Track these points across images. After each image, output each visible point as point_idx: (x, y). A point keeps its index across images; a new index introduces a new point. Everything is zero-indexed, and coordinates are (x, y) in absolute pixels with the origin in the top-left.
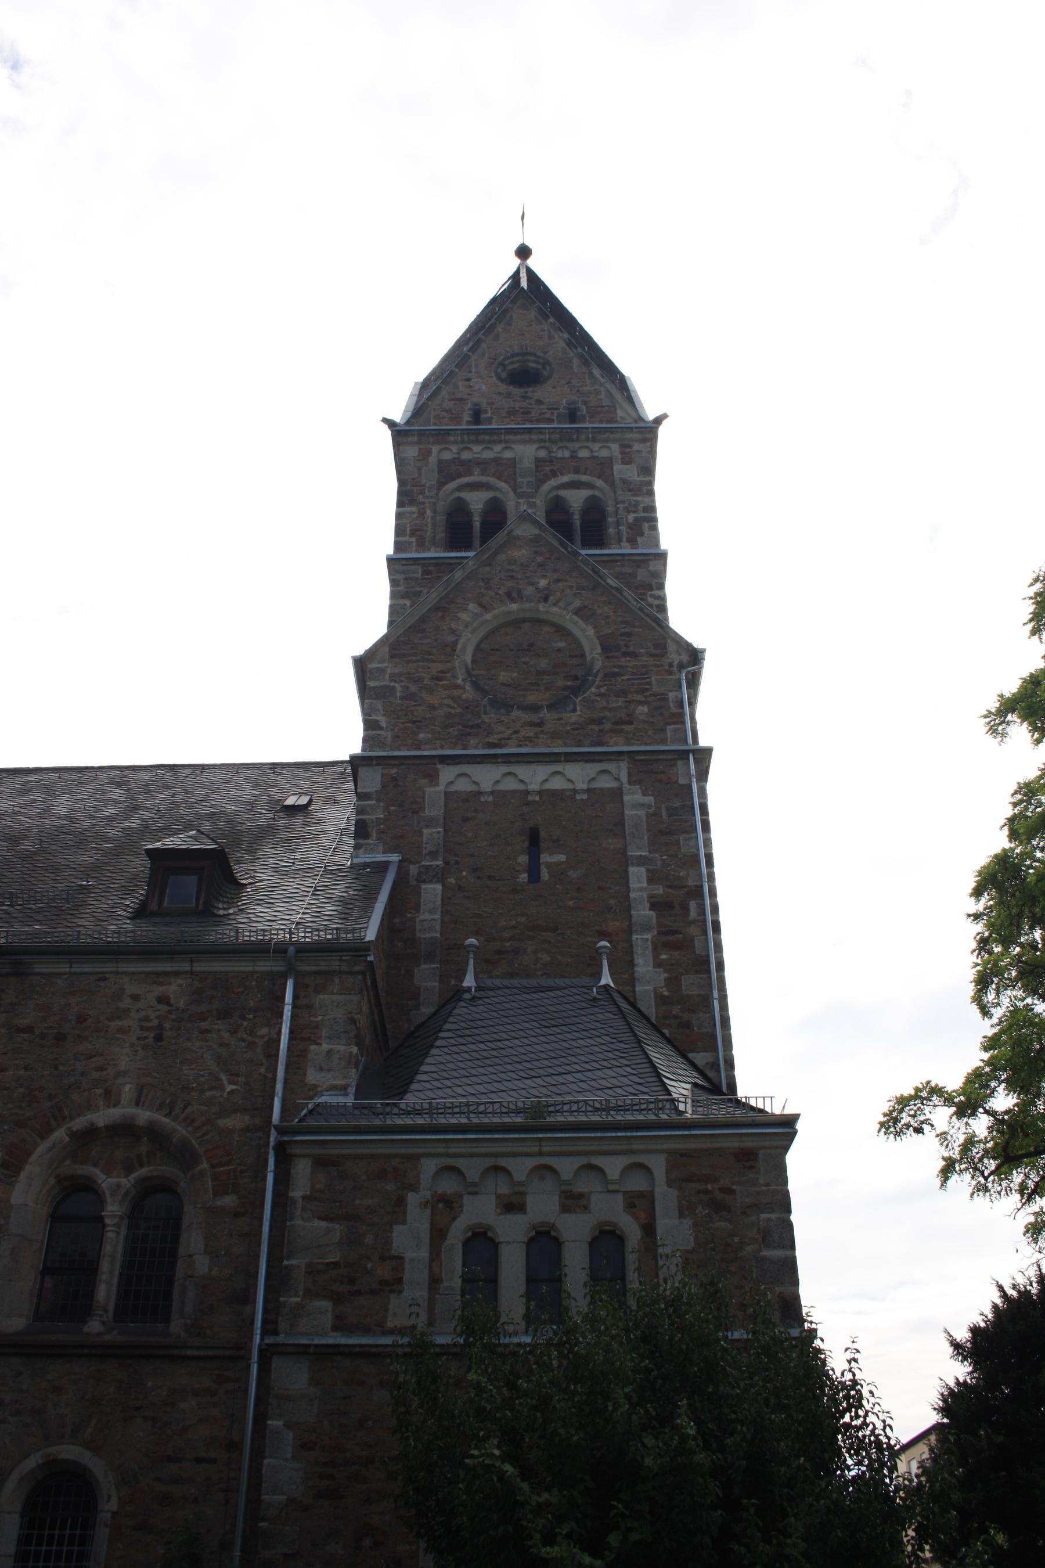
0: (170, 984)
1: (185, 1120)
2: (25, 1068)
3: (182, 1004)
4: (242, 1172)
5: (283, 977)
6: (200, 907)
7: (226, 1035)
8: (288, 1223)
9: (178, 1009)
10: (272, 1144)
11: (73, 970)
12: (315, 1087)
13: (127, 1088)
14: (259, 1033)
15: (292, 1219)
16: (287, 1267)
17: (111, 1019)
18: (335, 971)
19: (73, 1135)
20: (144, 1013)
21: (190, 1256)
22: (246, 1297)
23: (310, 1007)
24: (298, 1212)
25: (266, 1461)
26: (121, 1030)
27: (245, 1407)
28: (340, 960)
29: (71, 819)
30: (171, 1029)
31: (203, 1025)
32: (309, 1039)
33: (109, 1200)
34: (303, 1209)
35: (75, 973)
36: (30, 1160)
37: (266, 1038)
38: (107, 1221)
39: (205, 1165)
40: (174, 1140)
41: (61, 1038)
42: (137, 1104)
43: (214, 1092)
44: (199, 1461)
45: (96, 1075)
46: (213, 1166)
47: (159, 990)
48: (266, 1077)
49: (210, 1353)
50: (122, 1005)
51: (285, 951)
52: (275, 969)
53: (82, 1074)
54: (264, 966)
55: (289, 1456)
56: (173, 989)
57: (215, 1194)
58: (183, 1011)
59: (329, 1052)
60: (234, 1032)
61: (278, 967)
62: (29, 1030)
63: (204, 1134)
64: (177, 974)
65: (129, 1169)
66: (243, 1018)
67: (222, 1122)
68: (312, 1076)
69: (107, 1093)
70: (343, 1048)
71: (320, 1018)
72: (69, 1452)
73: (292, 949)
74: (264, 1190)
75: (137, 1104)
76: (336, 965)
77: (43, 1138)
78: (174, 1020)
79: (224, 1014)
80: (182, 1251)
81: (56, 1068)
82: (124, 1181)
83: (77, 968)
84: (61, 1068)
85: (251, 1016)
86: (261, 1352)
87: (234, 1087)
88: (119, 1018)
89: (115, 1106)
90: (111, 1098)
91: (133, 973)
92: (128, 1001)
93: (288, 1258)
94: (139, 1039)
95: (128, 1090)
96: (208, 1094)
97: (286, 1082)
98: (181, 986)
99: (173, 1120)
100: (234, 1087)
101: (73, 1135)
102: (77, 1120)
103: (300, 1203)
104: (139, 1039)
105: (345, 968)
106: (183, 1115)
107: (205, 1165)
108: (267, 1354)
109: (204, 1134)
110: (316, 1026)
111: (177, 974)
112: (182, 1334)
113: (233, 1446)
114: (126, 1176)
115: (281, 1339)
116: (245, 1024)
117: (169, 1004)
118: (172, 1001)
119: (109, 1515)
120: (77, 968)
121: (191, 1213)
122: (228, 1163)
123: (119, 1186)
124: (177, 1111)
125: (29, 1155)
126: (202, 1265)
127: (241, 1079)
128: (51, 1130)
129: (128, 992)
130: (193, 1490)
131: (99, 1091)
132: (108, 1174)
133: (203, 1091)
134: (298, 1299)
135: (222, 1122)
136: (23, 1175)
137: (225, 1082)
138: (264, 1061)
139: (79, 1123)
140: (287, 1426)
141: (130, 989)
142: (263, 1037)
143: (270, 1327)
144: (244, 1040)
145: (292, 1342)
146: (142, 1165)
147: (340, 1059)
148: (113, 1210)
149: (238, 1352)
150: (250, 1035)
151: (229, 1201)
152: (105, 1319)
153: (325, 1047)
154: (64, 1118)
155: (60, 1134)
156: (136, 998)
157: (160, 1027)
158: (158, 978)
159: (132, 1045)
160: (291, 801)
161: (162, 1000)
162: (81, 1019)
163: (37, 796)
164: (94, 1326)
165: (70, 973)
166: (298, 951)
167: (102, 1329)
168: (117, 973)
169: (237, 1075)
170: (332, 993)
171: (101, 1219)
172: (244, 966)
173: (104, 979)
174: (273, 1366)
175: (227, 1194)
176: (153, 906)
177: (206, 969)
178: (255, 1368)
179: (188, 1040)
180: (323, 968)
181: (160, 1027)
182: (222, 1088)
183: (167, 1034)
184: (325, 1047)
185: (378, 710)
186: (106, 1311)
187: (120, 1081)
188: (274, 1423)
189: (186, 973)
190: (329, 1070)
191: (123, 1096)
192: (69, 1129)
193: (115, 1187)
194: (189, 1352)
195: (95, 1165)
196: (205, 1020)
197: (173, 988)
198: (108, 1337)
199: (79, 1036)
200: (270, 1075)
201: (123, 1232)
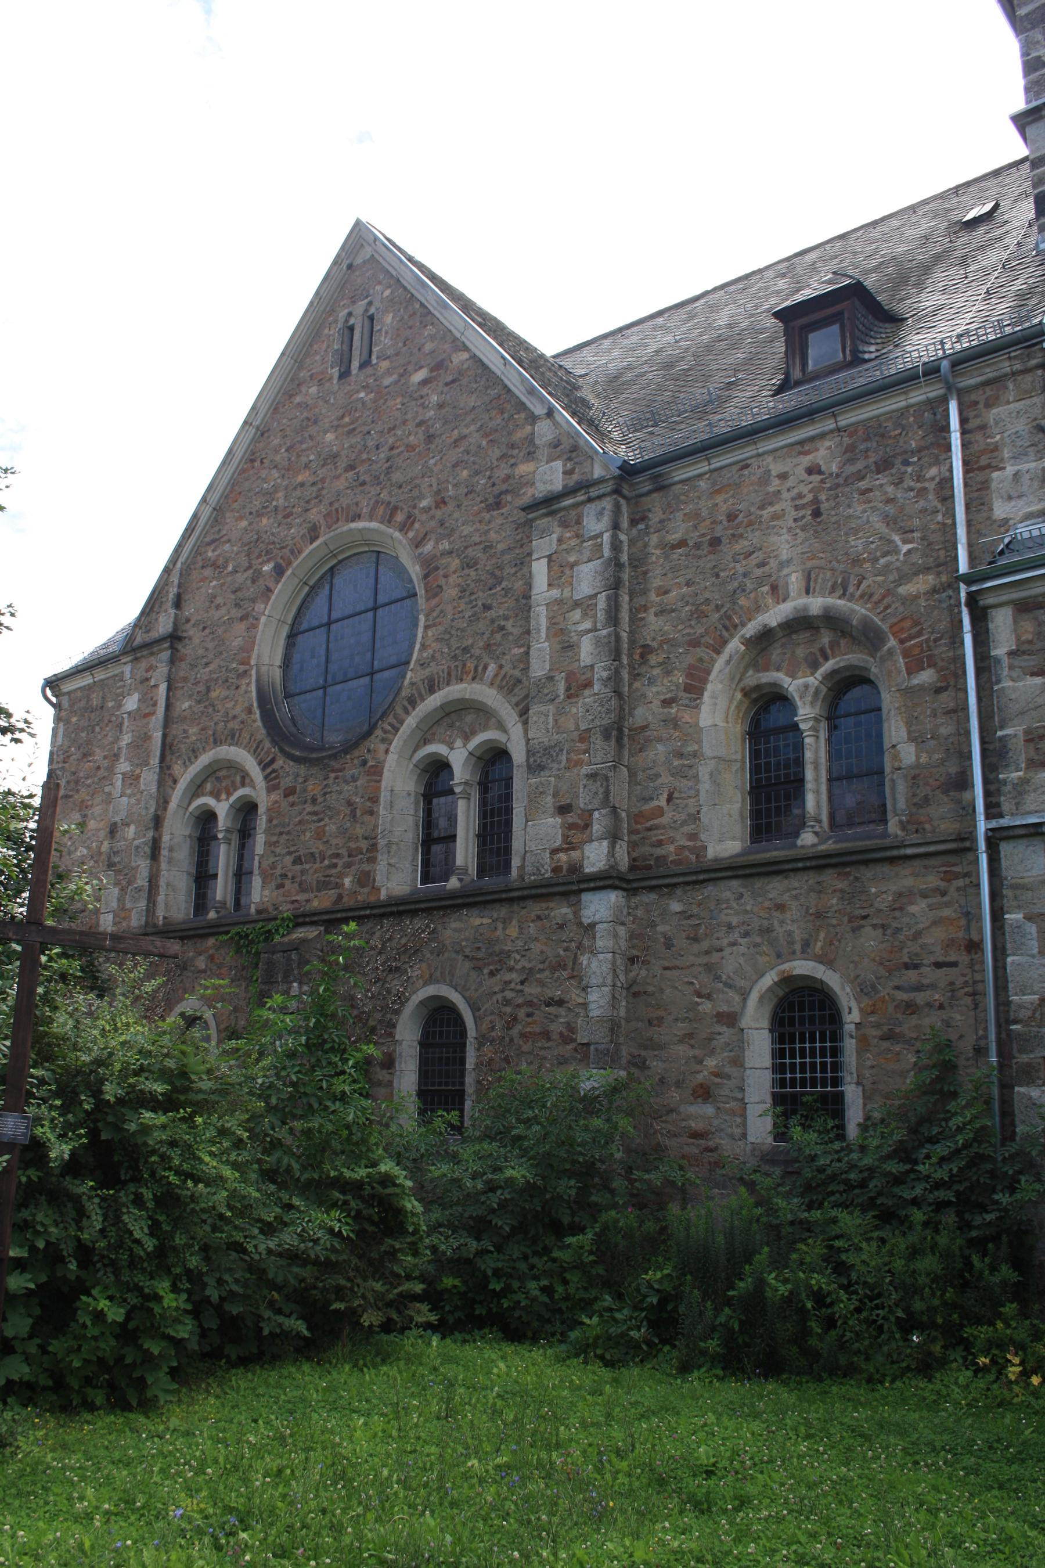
0: (817, 450)
1: (862, 596)
2: (688, 585)
3: (834, 469)
4: (936, 640)
5: (944, 400)
6: (848, 358)
7: (890, 489)
8: (996, 688)
9: (831, 475)
10: (963, 600)
11: (713, 466)
12: (1006, 521)
13: (793, 578)
14: (927, 476)
15: (998, 682)
16: (1001, 739)
17: (762, 508)
18: (1006, 375)
19: (748, 642)
20: (796, 491)
21: (894, 746)
22: (963, 782)
23: (983, 427)
24: (1006, 672)
25: (1009, 959)
26: (775, 517)
27: (979, 905)
28: (1010, 358)
29: (730, 326)
30: (828, 500)
31: (863, 485)
32: (989, 466)
33: (799, 703)
34: (1011, 667)
35: (716, 470)
36: (711, 677)
37: (937, 480)
38: (802, 726)
39: (892, 642)
40: (854, 622)
41: (715, 542)
42: (807, 592)
43: (888, 558)
44: (938, 965)
45: (758, 572)
46: (902, 642)
47: (806, 461)
48: (944, 524)
49: (932, 849)
50: (771, 489)
51: (937, 370)
52: (931, 395)
53: (745, 575)
54: (917, 396)
55: (1035, 951)
56: (824, 455)
57: (909, 673)
58: (838, 476)
59: (1016, 475)
60: (898, 483)
61: (935, 391)
62: (682, 543)
63: (886, 608)
64: (822, 436)
65: (814, 666)
66: (906, 463)
67: (902, 590)
68: (1000, 510)
69: (774, 588)
70: (1033, 465)
71: (998, 437)
72: (802, 967)
73: (945, 364)
74: (963, 656)
75: (807, 592)
76: (1006, 367)
77: (718, 652)
78: (830, 489)
79: (883, 466)
80: (887, 745)
81: (717, 576)
82: (811, 680)
83: (716, 463)
84: (722, 574)
85: (915, 459)
86: (989, 840)
87: (910, 546)
88: (771, 504)
89: (784, 601)
90: (778, 592)
91: (776, 450)
92: (777, 482)
93: (1002, 728)
94: (795, 520)
95: (795, 580)
96: (882, 561)
97: (969, 524)
98: (830, 448)
99: (849, 601)
100: (910, 546)
101: (748, 642)
102: (749, 626)
103: (1005, 661)
104: (795, 520)
105: (1018, 367)
106: (859, 593)
107: (892, 642)
108: (994, 840)
109: (886, 608)
110: (996, 448)
111: (822, 436)
112: (899, 832)
113: (974, 946)
114: (812, 674)
115: (1004, 822)
116: (909, 469)
117: (820, 472)
118: (823, 468)
119: (853, 1026)
120: (716, 463)
121: (888, 700)
122: (920, 634)
123: (806, 686)
124: (851, 589)
125: (709, 673)
126: (908, 754)
127: (916, 535)
128: (725, 642)
129: (774, 473)
130: (937, 997)
131: (766, 589)
132: (793, 676)
133: (876, 560)
134: (1021, 773)
135: (902, 590)
136: (706, 694)
137: (899, 543)
138: (939, 506)
139: (750, 629)
140: (1028, 918)
141: (776, 468)
142: (933, 479)
143: (993, 810)
144: (912, 490)
145: (1018, 823)
146: (826, 659)
147: (1031, 479)
148: (806, 713)
149: (962, 845)
150: (918, 481)
151: (926, 677)
152: (817, 829)
153: (1010, 470)
154: (735, 626)
155: (735, 645)
156: (783, 476)
157: (816, 501)
158: (803, 446)
159: (790, 530)
160: (970, 216)
161: (813, 470)
162: (731, 517)
163: (700, 319)
164: (807, 838)
165: (711, 471)
166: (954, 365)
167: (816, 840)
168: (759, 455)
169: (912, 531)
170: (1008, 403)
171: (795, 727)
172: (895, 403)
173: (747, 466)
174: (1002, 854)
175: (923, 669)
176: (797, 374)
177: (853, 420)
178: (984, 859)
179: (849, 506)
180: (991, 375)
181: (816, 501)
182: (896, 551)
183: (824, 506)
184: (1010, 470)
185: (1038, 42)
186: (819, 821)
187: (785, 571)
188: (1013, 917)
189: (831, 431)
190: (1019, 497)
191: (791, 587)
192: (743, 636)
193: (803, 688)
194: (909, 851)
195: (778, 670)
196: (863, 478)
197: (822, 452)
198: (823, 847)
199: (733, 535)
200: (949, 522)
201: (823, 735)
